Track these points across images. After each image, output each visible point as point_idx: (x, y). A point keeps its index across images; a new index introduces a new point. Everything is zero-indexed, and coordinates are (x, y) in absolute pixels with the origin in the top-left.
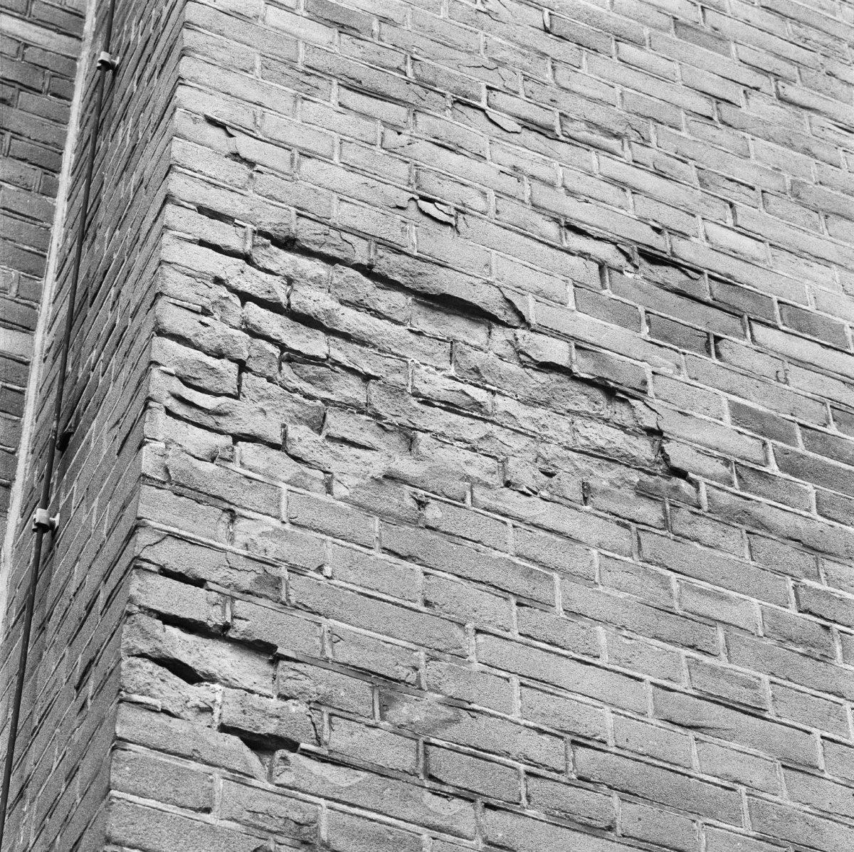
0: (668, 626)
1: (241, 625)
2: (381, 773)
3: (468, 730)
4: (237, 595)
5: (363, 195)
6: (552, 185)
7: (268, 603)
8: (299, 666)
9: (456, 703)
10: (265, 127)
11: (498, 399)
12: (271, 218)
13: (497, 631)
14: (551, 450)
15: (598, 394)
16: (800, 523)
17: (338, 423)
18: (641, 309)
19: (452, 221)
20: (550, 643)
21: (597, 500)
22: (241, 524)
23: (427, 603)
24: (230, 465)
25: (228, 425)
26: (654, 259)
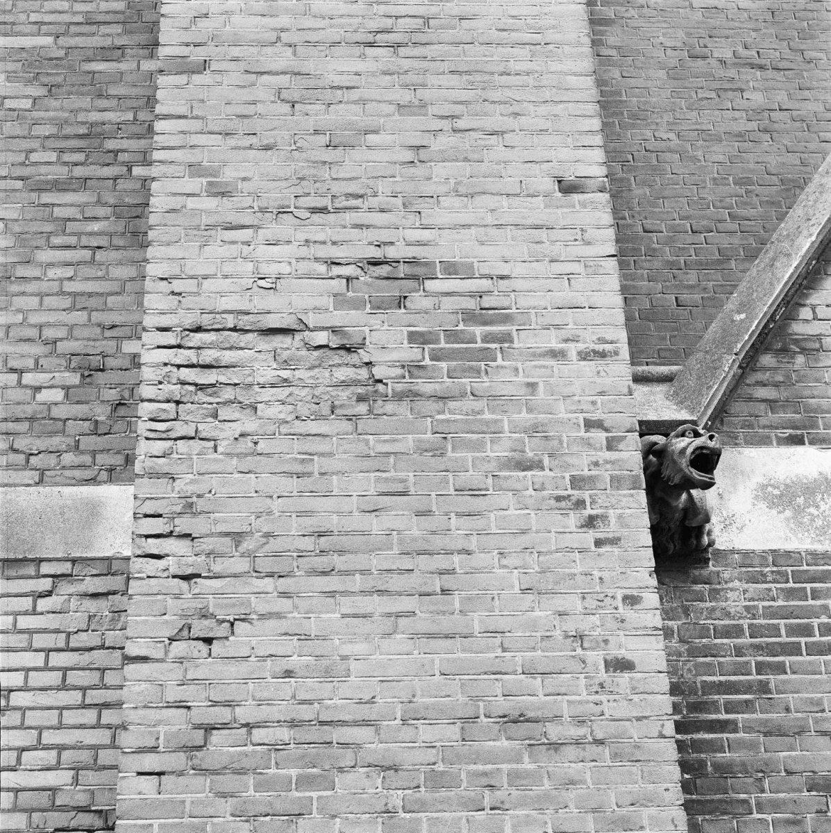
0: (367, 464)
1: (177, 529)
2: (235, 576)
3: (274, 545)
4: (175, 516)
5: (232, 290)
6: (324, 243)
7: (189, 515)
8: (201, 540)
9: (268, 535)
10: (186, 272)
11: (297, 372)
12: (190, 320)
13: (287, 494)
15: (342, 352)
16: (437, 386)
17: (224, 413)
18: (367, 297)
19: (274, 286)
20: (311, 492)
21: (337, 411)
23: (256, 492)
24: (172, 456)
25: (173, 435)
26: (375, 263)
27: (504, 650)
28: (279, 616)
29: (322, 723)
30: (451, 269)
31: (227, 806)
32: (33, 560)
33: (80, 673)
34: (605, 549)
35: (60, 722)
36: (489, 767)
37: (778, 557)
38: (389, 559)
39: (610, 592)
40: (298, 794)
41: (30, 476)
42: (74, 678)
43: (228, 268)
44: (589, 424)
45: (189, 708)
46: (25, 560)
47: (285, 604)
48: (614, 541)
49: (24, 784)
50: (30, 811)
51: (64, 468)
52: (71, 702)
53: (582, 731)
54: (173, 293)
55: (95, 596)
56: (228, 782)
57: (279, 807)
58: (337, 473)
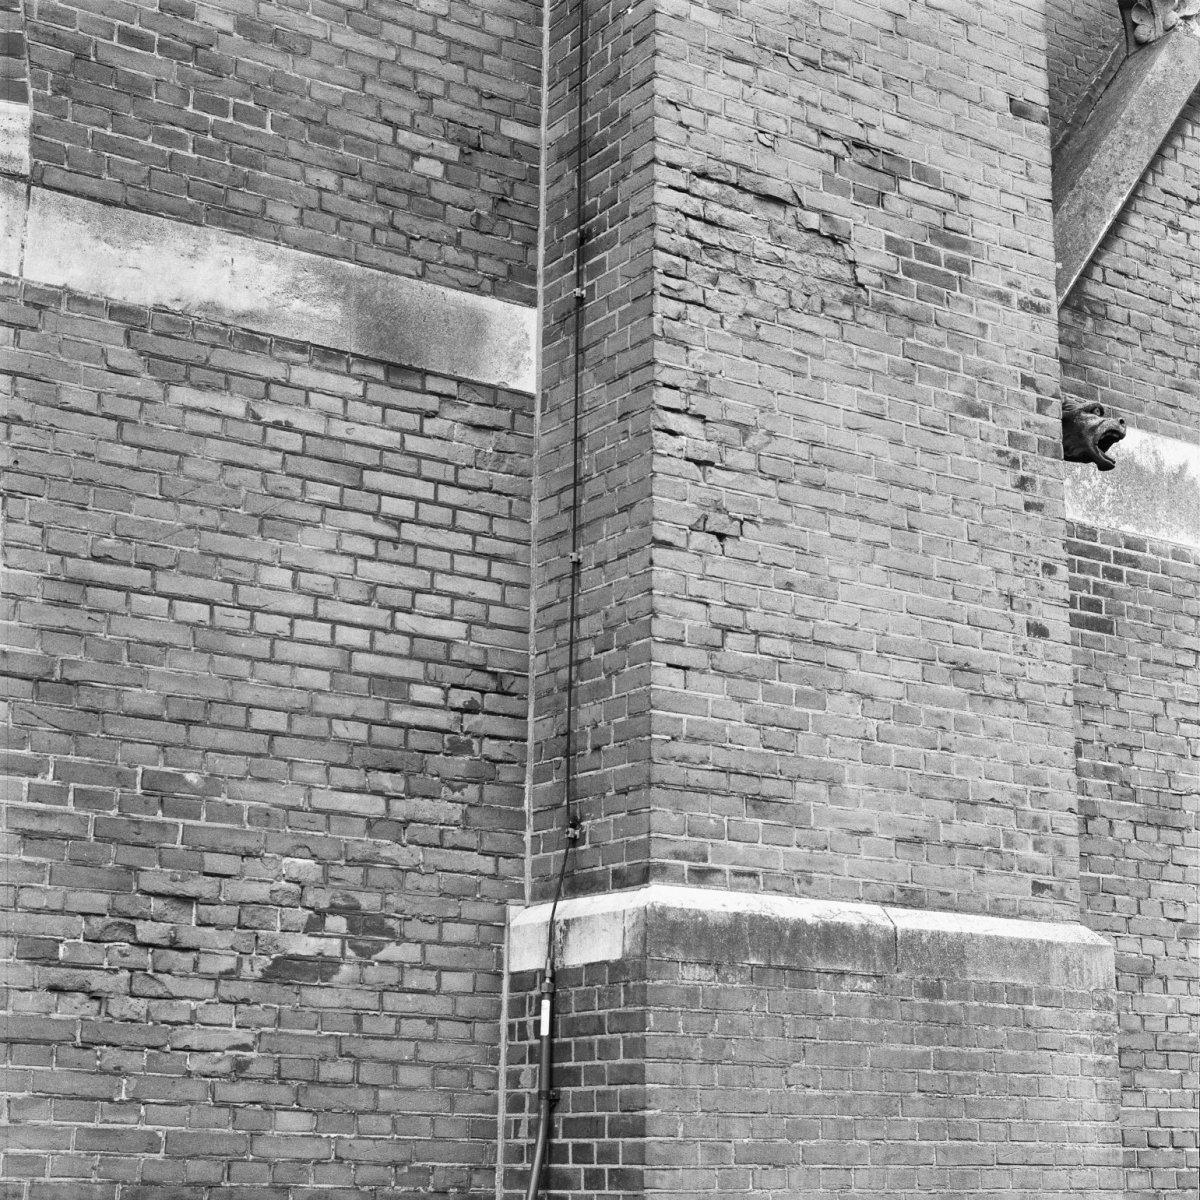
0: (853, 376)
2: (743, 472)
6: (816, 106)
9: (770, 434)
12: (698, 162)
14: (810, 280)
15: (829, 242)
21: (827, 310)
22: (691, 353)
25: (684, 297)
27: (955, 598)
28: (780, 523)
29: (816, 642)
30: (923, 175)
31: (740, 711)
32: (418, 371)
33: (470, 514)
34: (1032, 514)
35: (452, 567)
36: (941, 709)
37: (1082, 526)
38: (865, 483)
39: (1035, 557)
40: (797, 709)
41: (409, 265)
42: (466, 520)
43: (731, 109)
44: (1027, 382)
45: (707, 604)
46: (410, 368)
47: (784, 513)
48: (1039, 507)
49: (420, 630)
50: (426, 660)
51: (446, 264)
52: (462, 547)
53: (1009, 689)
54: (681, 123)
55: (478, 428)
56: (742, 687)
57: (784, 719)
58: (827, 380)
